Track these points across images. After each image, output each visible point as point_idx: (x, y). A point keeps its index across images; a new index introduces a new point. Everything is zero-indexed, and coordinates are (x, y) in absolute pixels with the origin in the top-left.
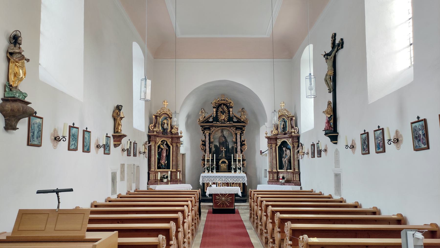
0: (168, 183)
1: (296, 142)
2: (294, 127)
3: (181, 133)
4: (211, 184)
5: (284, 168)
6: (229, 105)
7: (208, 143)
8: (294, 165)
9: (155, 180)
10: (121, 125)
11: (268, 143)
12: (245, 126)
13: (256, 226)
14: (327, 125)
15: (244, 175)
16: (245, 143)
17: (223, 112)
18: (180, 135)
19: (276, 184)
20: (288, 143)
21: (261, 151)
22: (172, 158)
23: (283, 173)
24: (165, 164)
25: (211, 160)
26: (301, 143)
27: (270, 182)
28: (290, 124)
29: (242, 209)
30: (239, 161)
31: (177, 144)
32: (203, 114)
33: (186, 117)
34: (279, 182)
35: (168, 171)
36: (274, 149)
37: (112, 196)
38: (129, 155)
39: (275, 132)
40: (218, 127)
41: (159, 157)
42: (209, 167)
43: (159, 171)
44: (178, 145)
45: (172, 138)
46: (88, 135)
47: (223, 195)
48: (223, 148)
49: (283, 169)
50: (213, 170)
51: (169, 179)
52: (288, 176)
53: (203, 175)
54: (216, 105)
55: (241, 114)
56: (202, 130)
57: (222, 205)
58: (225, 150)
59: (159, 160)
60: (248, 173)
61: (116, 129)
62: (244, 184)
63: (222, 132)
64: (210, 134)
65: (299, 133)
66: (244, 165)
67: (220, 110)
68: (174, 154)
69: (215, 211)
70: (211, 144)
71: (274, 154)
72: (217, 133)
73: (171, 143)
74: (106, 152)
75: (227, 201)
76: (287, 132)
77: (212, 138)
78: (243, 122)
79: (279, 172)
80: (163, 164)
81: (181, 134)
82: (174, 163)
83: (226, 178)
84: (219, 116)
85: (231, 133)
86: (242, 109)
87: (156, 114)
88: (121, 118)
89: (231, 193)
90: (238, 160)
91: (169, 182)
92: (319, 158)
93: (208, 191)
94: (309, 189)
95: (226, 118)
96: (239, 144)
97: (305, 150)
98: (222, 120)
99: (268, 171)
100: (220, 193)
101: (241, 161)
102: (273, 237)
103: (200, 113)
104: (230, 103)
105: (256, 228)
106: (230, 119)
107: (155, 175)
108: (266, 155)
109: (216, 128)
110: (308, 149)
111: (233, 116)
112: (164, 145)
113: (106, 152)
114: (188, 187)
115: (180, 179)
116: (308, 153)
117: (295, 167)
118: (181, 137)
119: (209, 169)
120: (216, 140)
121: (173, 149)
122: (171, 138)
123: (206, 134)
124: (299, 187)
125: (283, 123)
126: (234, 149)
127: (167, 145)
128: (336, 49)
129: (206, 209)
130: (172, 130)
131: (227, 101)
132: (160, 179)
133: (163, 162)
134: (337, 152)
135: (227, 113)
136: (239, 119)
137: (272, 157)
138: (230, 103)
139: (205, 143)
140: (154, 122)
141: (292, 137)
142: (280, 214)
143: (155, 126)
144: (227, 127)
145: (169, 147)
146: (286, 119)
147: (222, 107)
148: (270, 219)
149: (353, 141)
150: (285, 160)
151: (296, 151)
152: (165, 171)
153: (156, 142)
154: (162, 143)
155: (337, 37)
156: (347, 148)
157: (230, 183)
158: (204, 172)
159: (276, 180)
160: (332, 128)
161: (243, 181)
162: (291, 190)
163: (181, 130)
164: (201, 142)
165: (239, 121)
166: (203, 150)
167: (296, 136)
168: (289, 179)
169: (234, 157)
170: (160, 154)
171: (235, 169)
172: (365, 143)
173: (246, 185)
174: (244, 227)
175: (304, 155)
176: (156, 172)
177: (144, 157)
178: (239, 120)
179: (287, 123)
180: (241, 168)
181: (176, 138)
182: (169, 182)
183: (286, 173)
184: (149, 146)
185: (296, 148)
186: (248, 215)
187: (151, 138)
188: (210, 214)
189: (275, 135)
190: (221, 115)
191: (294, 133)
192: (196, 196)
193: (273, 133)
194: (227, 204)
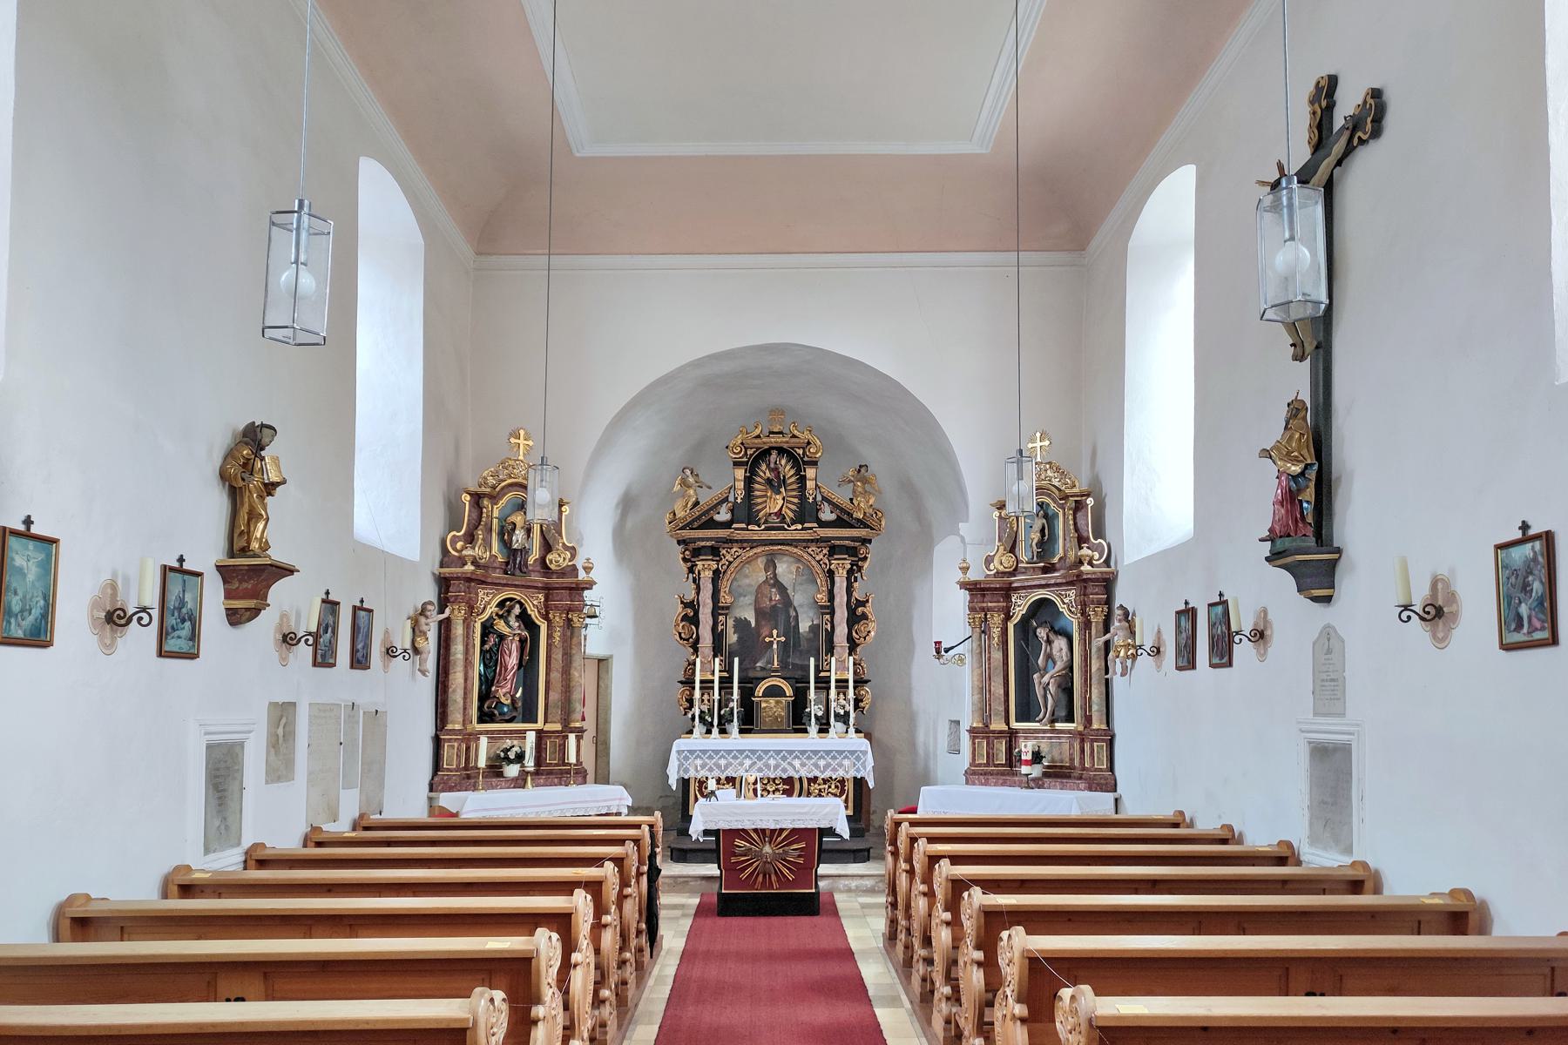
0: (525, 781)
1: (1099, 603)
2: (1088, 538)
3: (588, 569)
4: (712, 785)
5: (1041, 716)
7: (710, 611)
8: (1087, 703)
9: (466, 768)
10: (268, 519)
11: (972, 609)
12: (870, 541)
13: (921, 993)
14: (1283, 511)
15: (862, 744)
17: (776, 484)
18: (582, 575)
19: (1002, 785)
20: (1062, 608)
21: (938, 643)
22: (548, 674)
23: (1036, 738)
24: (514, 701)
25: (720, 683)
26: (1121, 606)
27: (974, 773)
28: (1072, 527)
29: (849, 890)
30: (842, 684)
31: (570, 616)
32: (692, 492)
33: (617, 505)
34: (1015, 774)
35: (525, 731)
36: (996, 632)
37: (212, 856)
38: (323, 659)
39: (1004, 562)
40: (754, 544)
41: (489, 670)
42: (709, 710)
43: (487, 732)
44: (575, 619)
45: (548, 590)
46: (41, 556)
47: (768, 833)
48: (775, 632)
49: (1037, 719)
51: (530, 763)
52: (1058, 749)
53: (681, 744)
55: (854, 491)
56: (685, 560)
57: (760, 878)
58: (783, 639)
59: (487, 683)
60: (876, 734)
61: (236, 535)
62: (859, 783)
63: (771, 564)
64: (716, 572)
65: (1112, 564)
66: (862, 704)
67: (761, 474)
68: (556, 660)
69: (728, 906)
70: (721, 618)
71: (997, 655)
73: (543, 611)
74: (172, 645)
75: (785, 860)
76: (1055, 560)
77: (727, 589)
78: (862, 524)
80: (503, 700)
81: (587, 573)
82: (555, 696)
83: (784, 759)
84: (759, 500)
85: (809, 568)
86: (859, 471)
87: (473, 488)
88: (265, 485)
89: (803, 826)
90: (837, 681)
91: (529, 778)
92: (1217, 670)
93: (700, 818)
94: (1165, 812)
95: (789, 508)
96: (841, 614)
97: (1145, 638)
98: (770, 514)
99: (966, 725)
100: (754, 827)
101: (847, 687)
102: (986, 1020)
103: (677, 488)
104: (809, 443)
105: (921, 1002)
106: (806, 512)
107: (468, 749)
108: (961, 659)
109: (744, 548)
110: (1159, 632)
111: (819, 498)
112: (510, 619)
113: (172, 645)
114: (615, 799)
115: (579, 762)
116: (1157, 651)
117: (1090, 710)
118: (589, 585)
119: (710, 720)
120: (742, 598)
121: (550, 636)
122: (543, 588)
124: (1110, 796)
125: (1039, 523)
126: (822, 636)
127: (524, 617)
128: (1338, 148)
129: (692, 892)
130: (550, 557)
131: (794, 436)
132: (489, 767)
133: (504, 690)
134: (1328, 645)
136: (842, 510)
137: (989, 668)
138: (809, 443)
139: (696, 613)
140: (469, 520)
141: (1079, 581)
143: (470, 538)
144: (791, 545)
146: (1052, 505)
147: (772, 460)
148: (1019, 1001)
149: (1440, 586)
150: (1046, 679)
151: (1098, 642)
152: (511, 732)
153: (473, 608)
154: (501, 613)
155: (1340, 94)
156: (1409, 618)
157: (800, 779)
158: (687, 733)
159: (1002, 765)
160: (1310, 524)
162: (1075, 813)
163: (587, 557)
164: (680, 610)
166: (688, 640)
167: (1099, 575)
169: (818, 671)
171: (824, 721)
172: (1526, 588)
173: (871, 785)
174: (856, 989)
175: (1134, 657)
176: (470, 734)
177: (413, 674)
178: (845, 517)
179: (1056, 523)
180: (847, 714)
181: (563, 588)
182: (529, 778)
183: (1050, 738)
184: (440, 622)
185: (1096, 627)
186: (880, 924)
187: (451, 589)
188: (707, 916)
189: (1003, 573)
191: (1090, 563)
192: (630, 852)
193: (996, 565)
194: (786, 871)
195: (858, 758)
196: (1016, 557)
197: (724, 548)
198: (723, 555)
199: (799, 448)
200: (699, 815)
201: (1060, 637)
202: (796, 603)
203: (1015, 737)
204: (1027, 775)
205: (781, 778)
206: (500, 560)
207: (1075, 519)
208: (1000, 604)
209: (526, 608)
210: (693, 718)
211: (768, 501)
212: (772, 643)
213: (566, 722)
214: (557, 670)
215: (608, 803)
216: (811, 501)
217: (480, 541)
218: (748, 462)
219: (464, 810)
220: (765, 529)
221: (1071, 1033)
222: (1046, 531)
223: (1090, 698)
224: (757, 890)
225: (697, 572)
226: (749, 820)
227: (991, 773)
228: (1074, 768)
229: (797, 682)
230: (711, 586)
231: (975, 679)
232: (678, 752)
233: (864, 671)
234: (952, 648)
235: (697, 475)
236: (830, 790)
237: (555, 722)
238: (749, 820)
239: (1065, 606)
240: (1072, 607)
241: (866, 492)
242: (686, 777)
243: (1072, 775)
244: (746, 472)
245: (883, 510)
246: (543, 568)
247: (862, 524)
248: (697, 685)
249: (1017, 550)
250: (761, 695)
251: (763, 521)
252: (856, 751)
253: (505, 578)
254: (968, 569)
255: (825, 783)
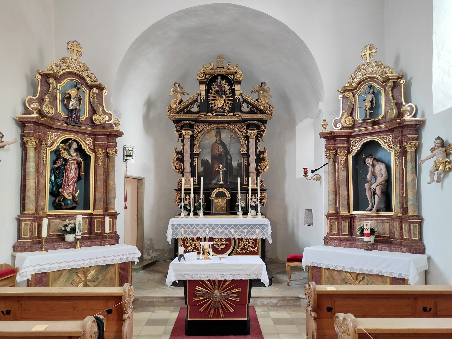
0: (76, 243)
6: (234, 77)
15: (266, 221)
16: (266, 155)
17: (220, 93)
19: (350, 247)
22: (95, 183)
25: (194, 190)
29: (264, 305)
31: (108, 151)
32: (179, 96)
33: (145, 104)
34: (354, 240)
35: (75, 215)
36: (342, 160)
40: (210, 122)
44: (111, 153)
47: (217, 283)
48: (221, 166)
50: (199, 210)
53: (174, 221)
54: (206, 77)
55: (259, 96)
57: (212, 311)
58: (225, 169)
62: (264, 241)
63: (218, 134)
64: (192, 137)
66: (263, 201)
67: (213, 89)
70: (195, 159)
71: (343, 174)
72: (207, 136)
75: (228, 300)
76: (380, 118)
77: (198, 145)
78: (262, 112)
79: (355, 217)
80: (67, 197)
81: (117, 127)
82: (100, 195)
83: (226, 228)
84: (212, 102)
86: (261, 85)
89: (239, 278)
96: (253, 157)
100: (208, 279)
103: (172, 93)
109: (206, 125)
111: (241, 100)
119: (189, 208)
121: (96, 162)
123: (184, 137)
127: (80, 150)
130: (95, 117)
131: (229, 69)
133: (68, 191)
135: (229, 95)
142: (317, 284)
145: (86, 158)
150: (374, 186)
154: (65, 147)
157: (234, 239)
161: (264, 235)
165: (254, 109)
166: (179, 170)
168: (384, 234)
170: (59, 172)
179: (379, 97)
180: (257, 206)
190: (216, 100)
195: (264, 229)
196: (353, 118)
197: (196, 125)
198: (195, 128)
199: (232, 75)
200: (172, 271)
201: (380, 163)
202: (231, 153)
203: (354, 219)
204: (368, 242)
205: (224, 238)
206: (62, 116)
207: (392, 93)
208: (344, 145)
209: (81, 145)
210: (181, 208)
211: (217, 102)
212: (219, 171)
213: (106, 211)
214: (101, 181)
215: (127, 256)
216: (237, 101)
217: (47, 103)
218: (207, 81)
219: (23, 266)
220: (216, 115)
221: (343, 333)
222: (374, 102)
223: (406, 197)
224: (210, 318)
225: (183, 137)
226: (205, 275)
227: (341, 240)
228: (394, 238)
229: (232, 190)
230: (189, 143)
231: (330, 187)
232: (173, 225)
233: (263, 185)
234: (316, 170)
235: (182, 88)
236: (249, 244)
237: (100, 210)
238: (205, 275)
239: (386, 144)
240: (390, 144)
241: (265, 96)
242: (176, 238)
243: (393, 242)
244: (206, 87)
245: (272, 105)
246: (92, 123)
247: (262, 112)
248: (183, 191)
249: (354, 114)
250: (214, 196)
251: (214, 112)
252: (263, 225)
253: (65, 126)
254: (327, 125)
255: (247, 241)
